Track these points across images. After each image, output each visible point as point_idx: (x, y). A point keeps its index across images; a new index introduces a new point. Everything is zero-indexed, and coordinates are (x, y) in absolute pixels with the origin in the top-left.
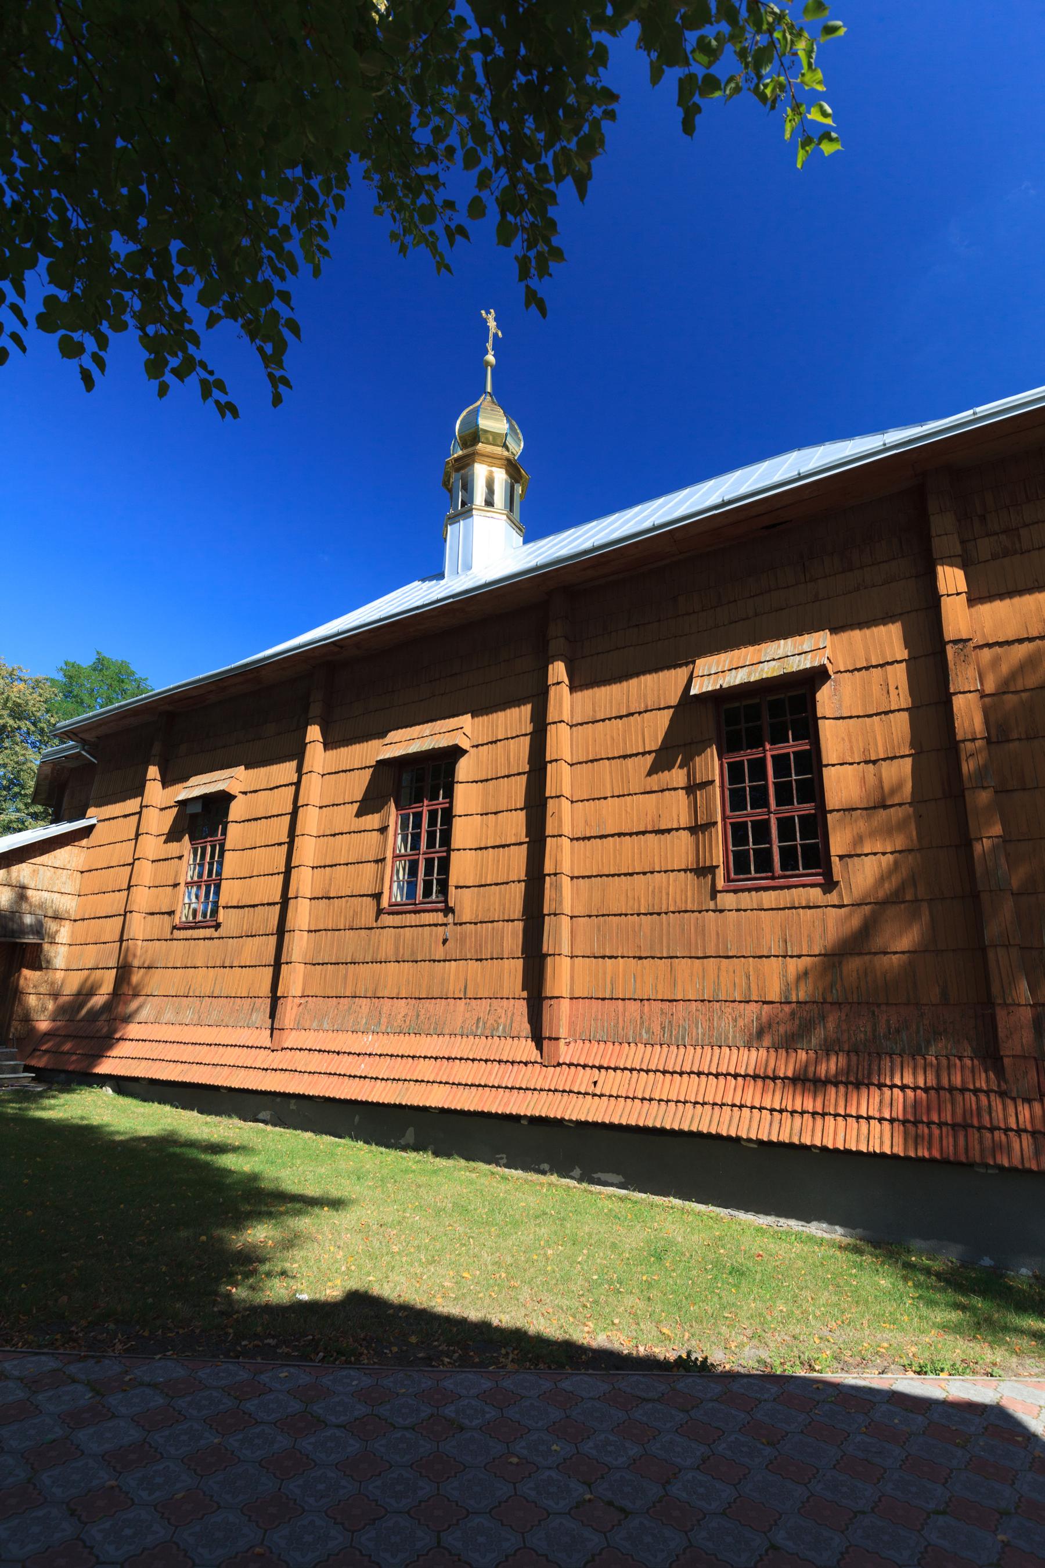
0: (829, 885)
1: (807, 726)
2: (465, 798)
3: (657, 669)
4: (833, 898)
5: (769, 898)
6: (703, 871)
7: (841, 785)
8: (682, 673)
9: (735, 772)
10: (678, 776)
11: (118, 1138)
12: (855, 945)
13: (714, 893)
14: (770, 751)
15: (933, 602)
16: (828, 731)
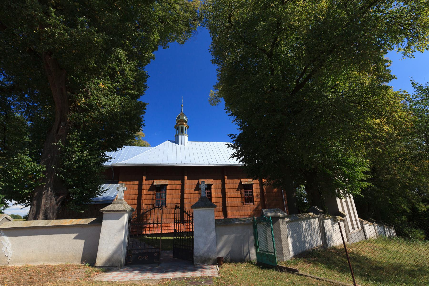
0: (254, 204)
1: (252, 188)
2: (213, 191)
6: (242, 202)
7: (255, 194)
8: (152, 181)
9: (245, 192)
10: (239, 192)
11: (127, 240)
12: (257, 208)
14: (249, 190)
15: (184, 179)
16: (254, 189)
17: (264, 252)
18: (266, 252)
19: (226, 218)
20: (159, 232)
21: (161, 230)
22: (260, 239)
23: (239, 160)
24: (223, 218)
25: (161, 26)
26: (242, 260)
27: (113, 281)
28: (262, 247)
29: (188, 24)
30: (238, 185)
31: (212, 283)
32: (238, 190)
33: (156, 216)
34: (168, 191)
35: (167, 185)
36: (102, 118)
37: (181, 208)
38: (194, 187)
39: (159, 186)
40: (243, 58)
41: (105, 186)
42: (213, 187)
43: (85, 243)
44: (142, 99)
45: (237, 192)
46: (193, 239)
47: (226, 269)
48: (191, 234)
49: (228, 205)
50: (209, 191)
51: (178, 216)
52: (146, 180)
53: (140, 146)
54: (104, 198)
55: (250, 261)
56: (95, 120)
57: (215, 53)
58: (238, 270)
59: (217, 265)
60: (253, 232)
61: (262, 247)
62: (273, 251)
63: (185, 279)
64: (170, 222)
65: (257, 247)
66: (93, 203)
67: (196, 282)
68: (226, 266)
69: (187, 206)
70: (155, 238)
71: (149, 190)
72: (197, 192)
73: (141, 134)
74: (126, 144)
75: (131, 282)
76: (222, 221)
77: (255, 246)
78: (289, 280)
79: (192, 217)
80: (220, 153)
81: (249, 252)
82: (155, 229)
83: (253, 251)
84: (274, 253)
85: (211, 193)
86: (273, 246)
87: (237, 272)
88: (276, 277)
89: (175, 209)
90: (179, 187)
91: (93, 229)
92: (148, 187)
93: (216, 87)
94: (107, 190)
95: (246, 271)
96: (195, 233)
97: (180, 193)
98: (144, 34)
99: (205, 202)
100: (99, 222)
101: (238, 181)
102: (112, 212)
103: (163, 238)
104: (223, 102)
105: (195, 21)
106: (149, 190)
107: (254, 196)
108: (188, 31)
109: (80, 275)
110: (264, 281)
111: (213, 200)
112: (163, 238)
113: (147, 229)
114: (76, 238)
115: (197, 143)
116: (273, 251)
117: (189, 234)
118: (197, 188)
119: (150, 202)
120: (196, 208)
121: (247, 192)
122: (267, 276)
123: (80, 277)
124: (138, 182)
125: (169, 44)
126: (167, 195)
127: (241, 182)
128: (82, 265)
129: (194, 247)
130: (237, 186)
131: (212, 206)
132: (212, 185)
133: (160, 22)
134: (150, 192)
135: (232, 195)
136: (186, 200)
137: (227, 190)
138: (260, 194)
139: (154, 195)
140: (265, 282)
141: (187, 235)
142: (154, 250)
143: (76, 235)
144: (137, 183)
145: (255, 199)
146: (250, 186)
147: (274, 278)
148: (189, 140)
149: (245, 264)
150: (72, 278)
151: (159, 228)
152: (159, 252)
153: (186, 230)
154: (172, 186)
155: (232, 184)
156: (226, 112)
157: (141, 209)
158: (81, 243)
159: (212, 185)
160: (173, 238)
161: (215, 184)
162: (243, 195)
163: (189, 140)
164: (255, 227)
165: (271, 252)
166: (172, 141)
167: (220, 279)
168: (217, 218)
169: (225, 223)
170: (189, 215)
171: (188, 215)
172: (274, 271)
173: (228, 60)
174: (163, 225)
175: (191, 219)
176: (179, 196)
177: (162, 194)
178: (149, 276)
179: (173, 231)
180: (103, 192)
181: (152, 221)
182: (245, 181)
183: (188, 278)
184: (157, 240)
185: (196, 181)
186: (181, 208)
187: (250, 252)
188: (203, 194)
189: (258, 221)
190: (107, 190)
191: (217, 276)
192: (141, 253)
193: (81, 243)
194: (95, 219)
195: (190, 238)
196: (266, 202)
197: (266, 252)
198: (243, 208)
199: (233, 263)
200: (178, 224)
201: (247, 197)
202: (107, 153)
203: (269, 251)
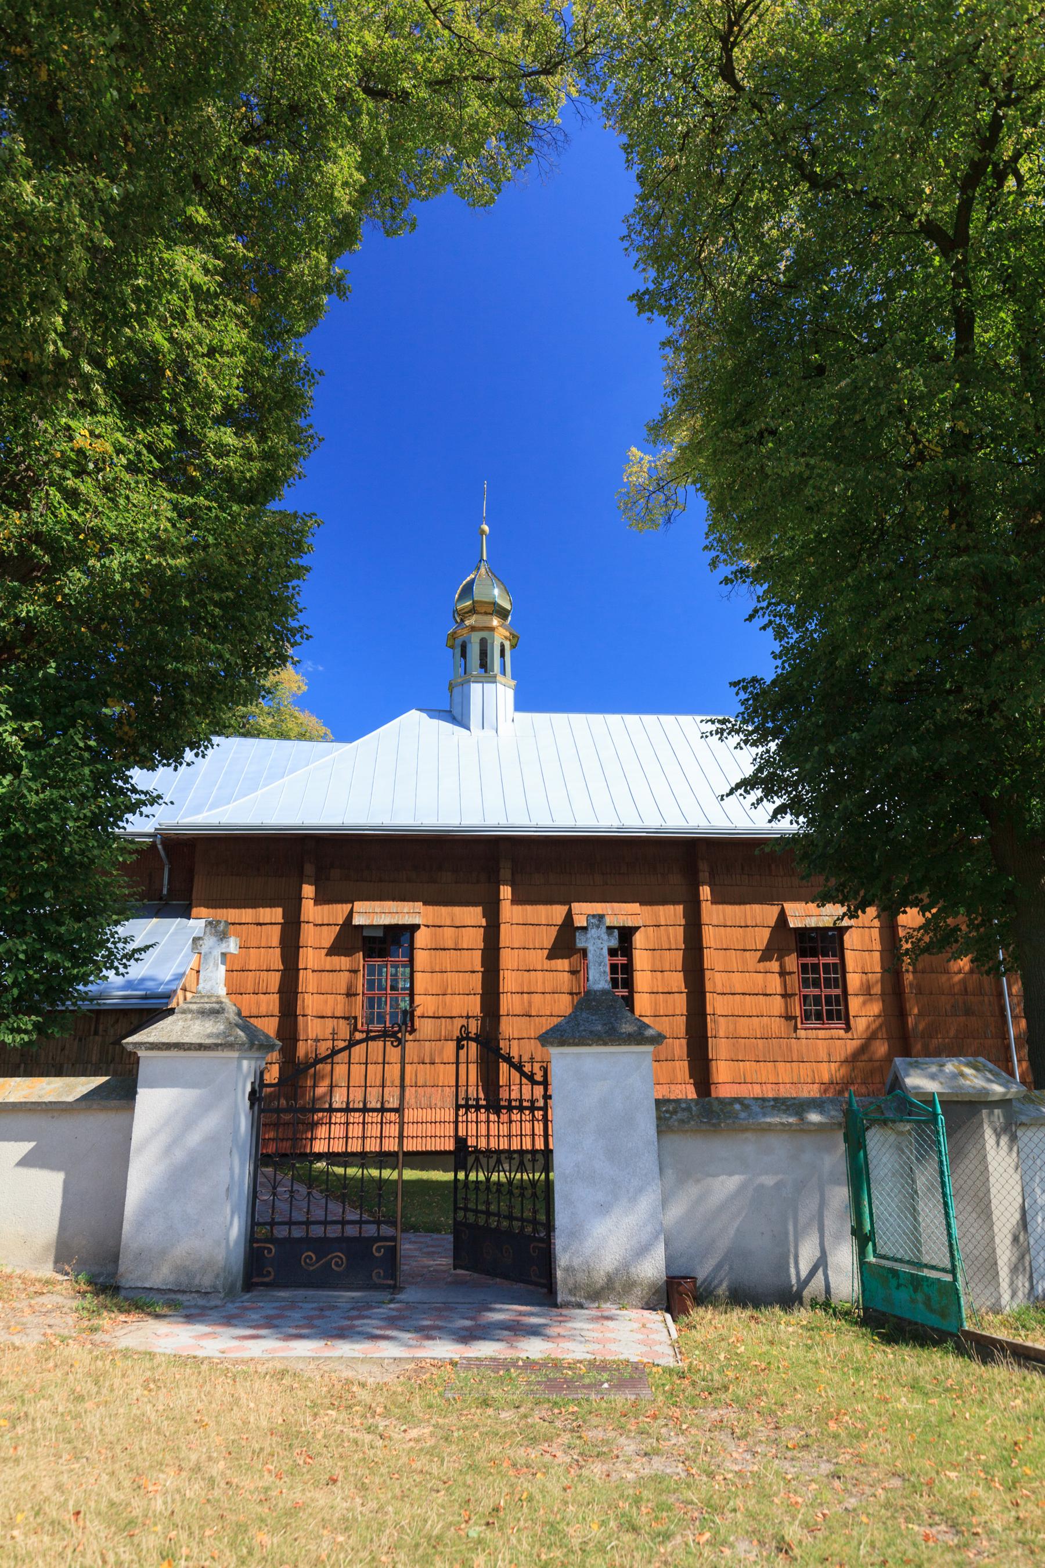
0: (848, 1028)
2: (641, 959)
3: (381, 900)
4: (849, 1035)
5: (821, 1033)
6: (789, 1018)
7: (854, 981)
9: (804, 968)
10: (775, 966)
12: (863, 1049)
13: (796, 1029)
14: (824, 960)
15: (497, 901)
16: (848, 954)
17: (897, 1266)
18: (909, 1262)
19: (709, 1094)
20: (390, 1145)
21: (401, 1137)
22: (884, 1200)
23: (769, 807)
24: (691, 1093)
25: (374, 116)
26: (788, 1298)
27: (201, 1354)
28: (891, 1241)
29: (518, 91)
30: (766, 933)
31: (646, 1394)
32: (766, 955)
33: (374, 1070)
34: (421, 958)
35: (415, 927)
36: (103, 608)
37: (486, 1042)
38: (548, 937)
39: (380, 934)
40: (808, 268)
41: (138, 930)
42: (638, 939)
43: (66, 1185)
44: (287, 501)
45: (761, 966)
46: (549, 1185)
47: (712, 1335)
48: (541, 1160)
49: (718, 1028)
50: (621, 960)
51: (472, 1073)
52: (319, 900)
53: (283, 736)
54: (130, 985)
55: (825, 1304)
56: (69, 612)
57: (659, 256)
58: (772, 1343)
59: (668, 1310)
60: (843, 1167)
61: (891, 1241)
62: (947, 1263)
63: (518, 1367)
64: (436, 1099)
65: (863, 1238)
66: (85, 1006)
67: (569, 1383)
68: (709, 1323)
69: (516, 1033)
70: (375, 1173)
71: (332, 951)
72: (563, 964)
73: (289, 680)
74: (222, 729)
75: (279, 1366)
76: (688, 1109)
77: (854, 1232)
78: (1026, 1401)
79: (545, 1083)
80: (682, 772)
81: (821, 1263)
82: (374, 1130)
83: (844, 1256)
84: (953, 1271)
85: (628, 969)
86: (944, 1239)
87: (766, 1348)
88: (960, 1383)
89: (459, 1047)
90: (475, 938)
91: (98, 1123)
92: (328, 936)
93: (658, 431)
94: (146, 948)
95: (809, 1348)
96: (560, 1159)
97: (479, 967)
98: (288, 159)
99: (603, 1016)
100: (122, 1090)
101: (768, 913)
102: (173, 1053)
103: (410, 1174)
104: (696, 507)
105: (547, 72)
106: (332, 951)
107: (850, 990)
108: (515, 135)
109: (55, 1319)
110: (898, 1400)
111: (642, 1003)
112: (410, 1174)
113: (322, 1132)
114: (25, 1162)
115: (560, 719)
116: (947, 1263)
117: (483, 1160)
118: (566, 943)
119: (337, 1005)
120: (562, 1043)
121: (815, 968)
122: (916, 1379)
123: (57, 1330)
124: (279, 911)
125: (415, 209)
126: (418, 977)
127: (782, 917)
128: (60, 1277)
129: (557, 1224)
130: (762, 937)
131: (640, 1037)
132: (637, 928)
133: (367, 91)
134: (335, 959)
135: (738, 981)
136: (507, 1003)
137: (711, 958)
138: (883, 980)
139: (355, 972)
140: (904, 1402)
141: (522, 1168)
142: (370, 1230)
143: (26, 1147)
144: (276, 914)
145: (855, 1004)
146: (829, 940)
147: (947, 1390)
148: (521, 705)
149: (803, 1315)
150: (23, 1329)
151: (393, 1130)
152: (393, 1239)
153: (493, 1145)
154: (443, 932)
155: (736, 929)
156: (714, 564)
157: (296, 1040)
158: (48, 1187)
159: (635, 929)
160: (449, 1176)
161: (656, 926)
162: (794, 981)
163: (521, 705)
164: (856, 1145)
165: (933, 1268)
166: (435, 713)
167: (682, 1376)
168: (662, 1092)
169: (700, 1113)
170: (531, 1078)
171: (523, 1074)
172: (951, 1358)
173: (722, 282)
174: (409, 1115)
175: (539, 1090)
176: (476, 982)
177: (389, 969)
178: (305, 1348)
179: (450, 1145)
180: (129, 956)
181: (339, 1099)
182: (804, 915)
183: (530, 1365)
184: (381, 1182)
185: (557, 913)
186: (486, 1042)
187: (831, 1260)
188: (599, 977)
189: (866, 1107)
190: (146, 948)
191: (671, 1362)
192: (322, 1245)
193: (48, 1187)
194: (103, 1079)
195: (533, 1183)
196: (911, 1020)
197: (909, 1262)
198: (790, 1049)
199: (745, 1306)
200: (472, 1116)
201: (816, 991)
202: (138, 776)
203: (926, 1259)
